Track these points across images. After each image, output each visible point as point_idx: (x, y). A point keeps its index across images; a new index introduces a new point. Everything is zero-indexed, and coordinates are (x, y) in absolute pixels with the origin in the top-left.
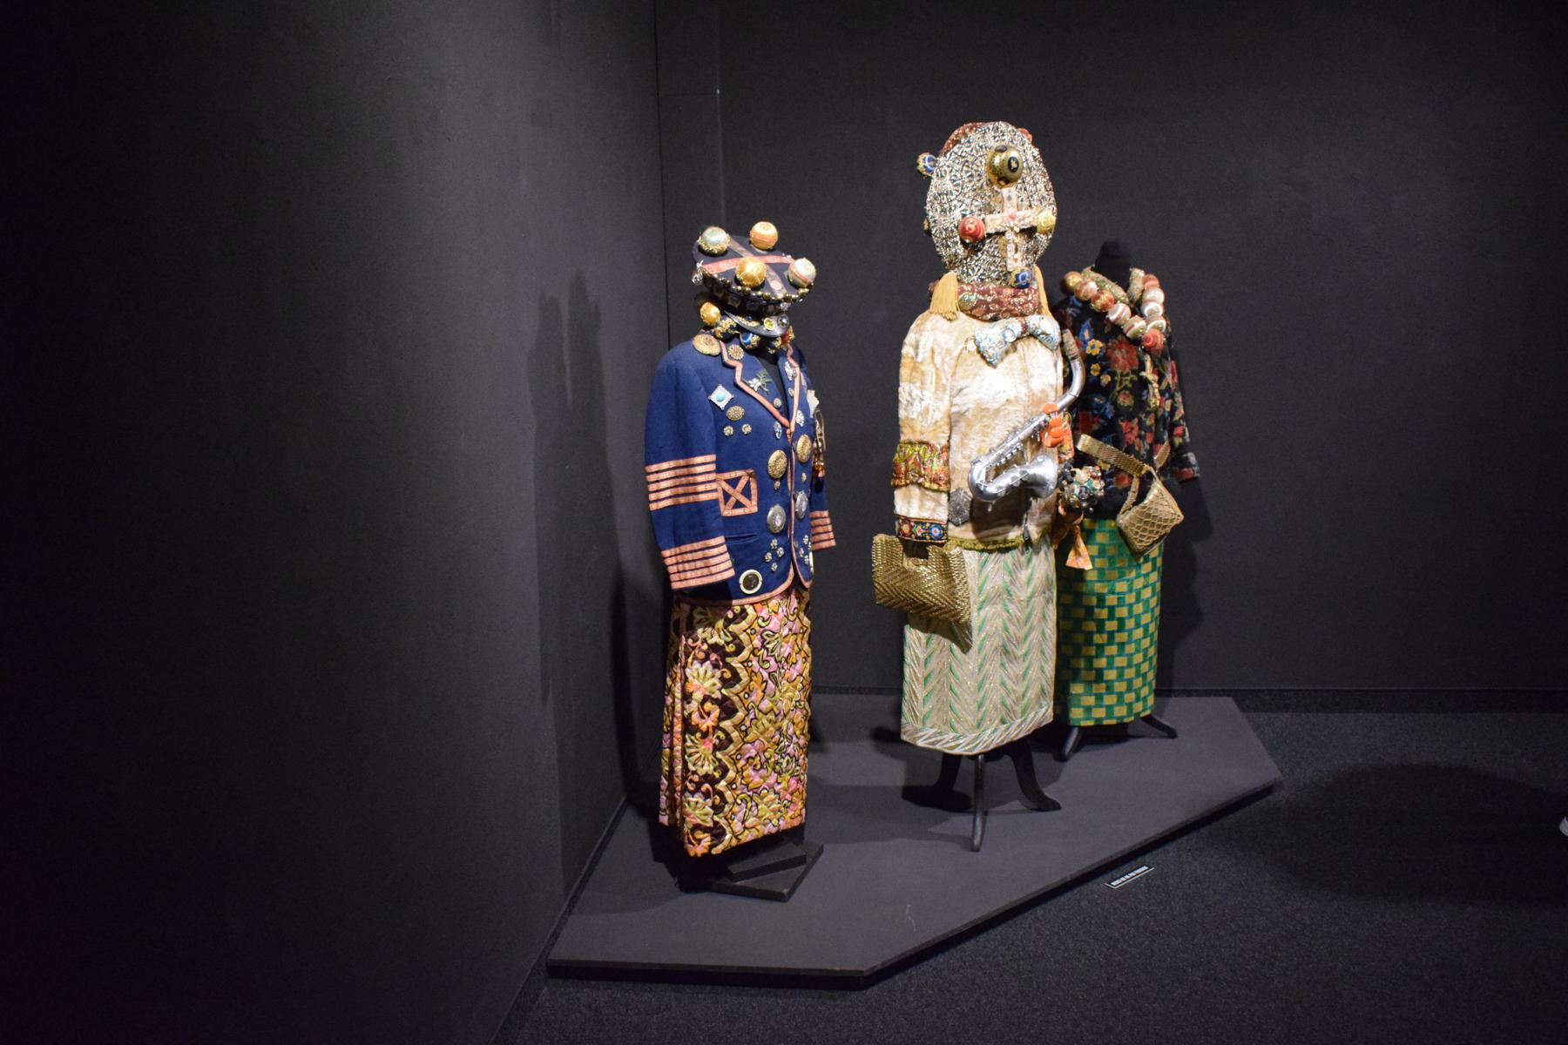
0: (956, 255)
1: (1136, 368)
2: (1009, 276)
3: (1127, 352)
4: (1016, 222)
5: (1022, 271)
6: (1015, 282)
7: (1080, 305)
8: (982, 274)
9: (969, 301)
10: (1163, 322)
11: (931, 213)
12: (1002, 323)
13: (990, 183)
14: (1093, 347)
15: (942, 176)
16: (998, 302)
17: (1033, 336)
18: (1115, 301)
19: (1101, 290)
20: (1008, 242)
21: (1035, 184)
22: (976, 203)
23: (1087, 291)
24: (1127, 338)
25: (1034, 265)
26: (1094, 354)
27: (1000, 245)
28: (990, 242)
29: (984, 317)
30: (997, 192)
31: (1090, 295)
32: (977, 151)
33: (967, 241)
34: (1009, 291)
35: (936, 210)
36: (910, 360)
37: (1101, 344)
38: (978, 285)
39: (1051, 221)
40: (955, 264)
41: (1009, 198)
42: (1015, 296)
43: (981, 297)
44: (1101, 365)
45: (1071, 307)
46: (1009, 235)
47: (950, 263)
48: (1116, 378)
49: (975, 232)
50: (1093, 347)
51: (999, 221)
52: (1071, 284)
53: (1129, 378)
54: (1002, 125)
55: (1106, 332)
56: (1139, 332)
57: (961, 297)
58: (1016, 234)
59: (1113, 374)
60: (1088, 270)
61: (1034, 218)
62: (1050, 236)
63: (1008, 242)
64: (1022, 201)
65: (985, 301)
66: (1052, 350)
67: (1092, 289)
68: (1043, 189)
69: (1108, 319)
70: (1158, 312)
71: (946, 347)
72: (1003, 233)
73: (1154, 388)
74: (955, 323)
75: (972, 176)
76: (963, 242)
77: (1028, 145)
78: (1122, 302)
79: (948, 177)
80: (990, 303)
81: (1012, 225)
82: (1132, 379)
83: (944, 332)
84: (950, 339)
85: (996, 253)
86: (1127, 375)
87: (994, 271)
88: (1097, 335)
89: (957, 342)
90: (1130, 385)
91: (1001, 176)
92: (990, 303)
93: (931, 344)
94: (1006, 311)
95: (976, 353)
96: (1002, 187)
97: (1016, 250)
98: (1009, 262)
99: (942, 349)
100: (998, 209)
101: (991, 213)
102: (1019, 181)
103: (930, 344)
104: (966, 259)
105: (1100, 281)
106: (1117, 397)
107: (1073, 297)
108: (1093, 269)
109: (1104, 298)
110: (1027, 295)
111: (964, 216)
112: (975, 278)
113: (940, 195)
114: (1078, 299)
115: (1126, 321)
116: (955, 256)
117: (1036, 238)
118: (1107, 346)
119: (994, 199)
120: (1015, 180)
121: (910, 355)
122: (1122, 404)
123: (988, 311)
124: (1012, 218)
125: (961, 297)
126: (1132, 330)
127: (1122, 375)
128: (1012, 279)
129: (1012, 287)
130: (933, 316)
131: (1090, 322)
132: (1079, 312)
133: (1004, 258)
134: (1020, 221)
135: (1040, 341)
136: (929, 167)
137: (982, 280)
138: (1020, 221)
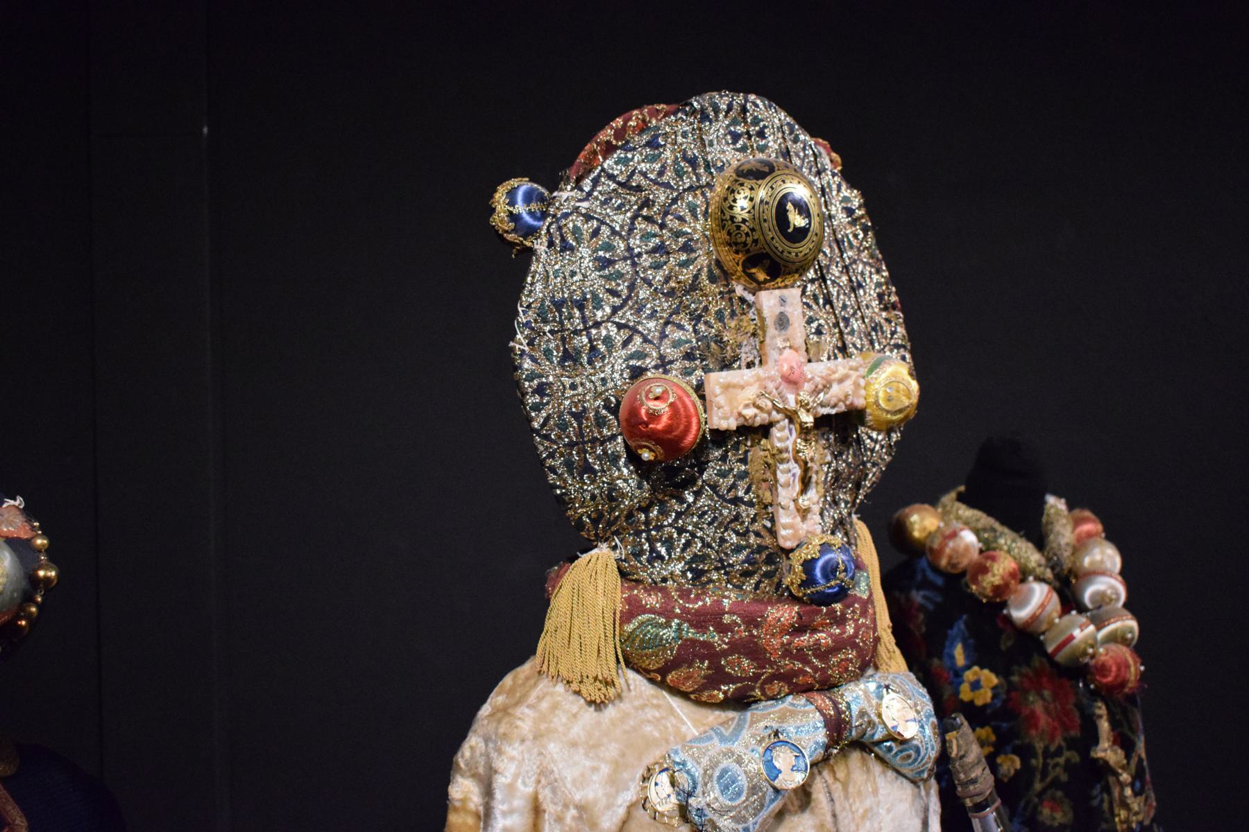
0: (613, 496)
1: (1075, 733)
2: (784, 563)
3: (1056, 696)
4: (804, 396)
5: (826, 547)
6: (804, 584)
7: (939, 581)
8: (696, 558)
9: (658, 643)
10: (1130, 624)
11: (527, 364)
12: (765, 716)
13: (720, 273)
14: (976, 685)
15: (566, 247)
16: (753, 650)
17: (863, 745)
18: (1022, 574)
19: (988, 549)
20: (778, 456)
21: (855, 287)
22: (678, 335)
23: (955, 550)
24: (1054, 664)
25: (854, 517)
26: (979, 702)
27: (755, 467)
28: (724, 458)
29: (705, 697)
30: (742, 300)
31: (964, 562)
32: (679, 174)
33: (646, 455)
34: (785, 614)
35: (548, 353)
36: (470, 821)
37: (995, 680)
38: (685, 594)
39: (908, 394)
40: (610, 524)
41: (783, 322)
42: (799, 629)
43: (691, 633)
44: (996, 730)
45: (919, 588)
46: (784, 437)
47: (595, 522)
48: (1034, 762)
49: (669, 429)
50: (976, 685)
51: (751, 393)
52: (916, 534)
53: (1061, 760)
54: (758, 106)
55: (1003, 647)
56: (1085, 653)
57: (629, 628)
58: (804, 432)
59: (1025, 753)
60: (949, 498)
61: (857, 385)
62: (895, 437)
63: (778, 456)
64: (819, 332)
65: (708, 645)
66: (913, 782)
67: (967, 548)
68: (875, 303)
69: (1008, 620)
70: (1118, 599)
71: (578, 797)
72: (765, 430)
73: (1122, 785)
74: (610, 712)
75: (661, 249)
76: (633, 458)
77: (831, 178)
78: (1039, 579)
79: (584, 251)
80: (725, 654)
81: (792, 404)
82: (1068, 760)
83: (574, 744)
84: (595, 769)
85: (741, 494)
86: (1058, 753)
87: (738, 549)
88: (979, 657)
89: (615, 783)
90: (1064, 778)
91: (754, 250)
92: (725, 654)
93: (530, 790)
94: (773, 677)
95: (676, 821)
96: (760, 286)
97: (806, 483)
98: (784, 519)
99: (566, 806)
100: (746, 355)
101: (726, 365)
102: (811, 274)
103: (525, 789)
104: (646, 510)
105: (985, 530)
106: (1035, 808)
107: (923, 563)
108: (961, 498)
109: (1002, 567)
110: (841, 621)
111: (637, 373)
112: (678, 567)
113: (559, 305)
114: (936, 569)
115: (1051, 624)
116: (611, 498)
117: (859, 441)
118: (1009, 683)
119: (733, 324)
120: (801, 269)
121: (472, 806)
122: (1048, 823)
123: (717, 677)
124: (792, 381)
125: (629, 628)
126: (1066, 650)
127: (1047, 754)
128: (792, 578)
129: (794, 599)
130: (544, 684)
131: (966, 624)
132: (939, 599)
133: (766, 509)
134: (816, 392)
135: (878, 757)
136: (527, 218)
137: (698, 574)
138: (816, 392)
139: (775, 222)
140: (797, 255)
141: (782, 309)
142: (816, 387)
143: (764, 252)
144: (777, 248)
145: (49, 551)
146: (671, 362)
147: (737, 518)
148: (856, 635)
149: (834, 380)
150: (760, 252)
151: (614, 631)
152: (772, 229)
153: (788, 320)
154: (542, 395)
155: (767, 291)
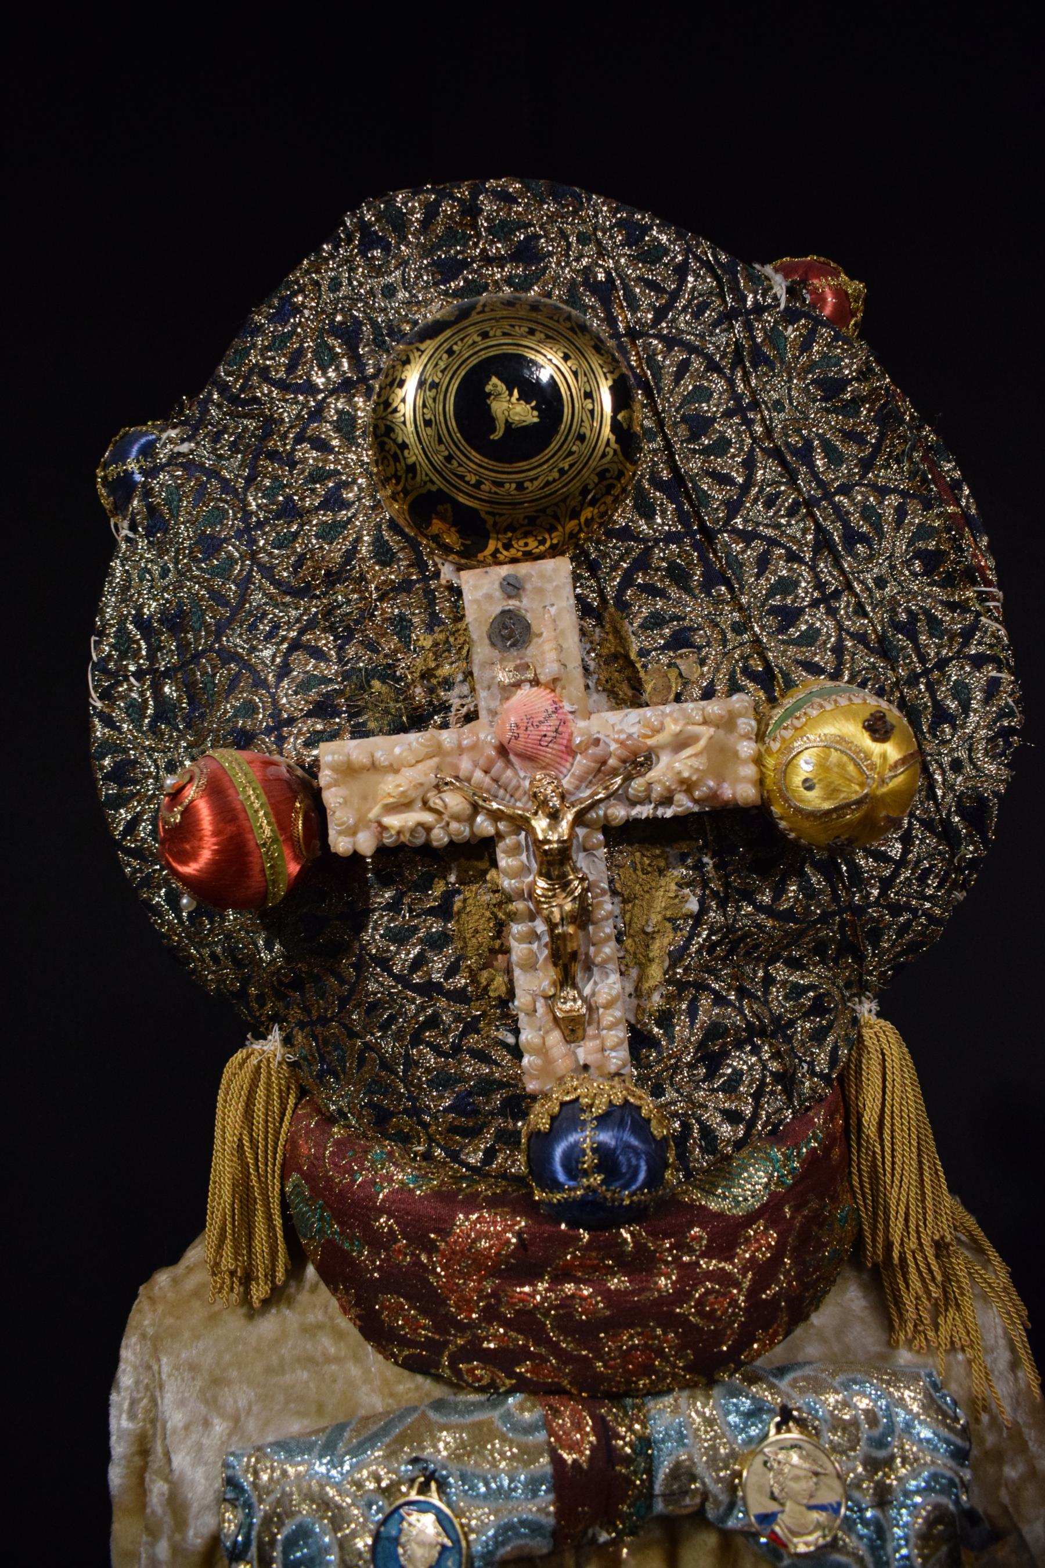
139: (453, 424)
140: (520, 486)
141: (512, 604)
142: (604, 763)
143: (434, 488)
144: (462, 478)
145: (367, 870)
146: (291, 721)
147: (434, 1021)
148: (681, 1295)
149: (662, 747)
150: (423, 491)
151: (884, 1099)
152: (446, 438)
153: (528, 626)
154: (122, 782)
155: (471, 572)
